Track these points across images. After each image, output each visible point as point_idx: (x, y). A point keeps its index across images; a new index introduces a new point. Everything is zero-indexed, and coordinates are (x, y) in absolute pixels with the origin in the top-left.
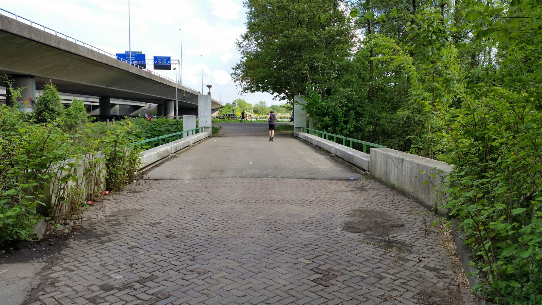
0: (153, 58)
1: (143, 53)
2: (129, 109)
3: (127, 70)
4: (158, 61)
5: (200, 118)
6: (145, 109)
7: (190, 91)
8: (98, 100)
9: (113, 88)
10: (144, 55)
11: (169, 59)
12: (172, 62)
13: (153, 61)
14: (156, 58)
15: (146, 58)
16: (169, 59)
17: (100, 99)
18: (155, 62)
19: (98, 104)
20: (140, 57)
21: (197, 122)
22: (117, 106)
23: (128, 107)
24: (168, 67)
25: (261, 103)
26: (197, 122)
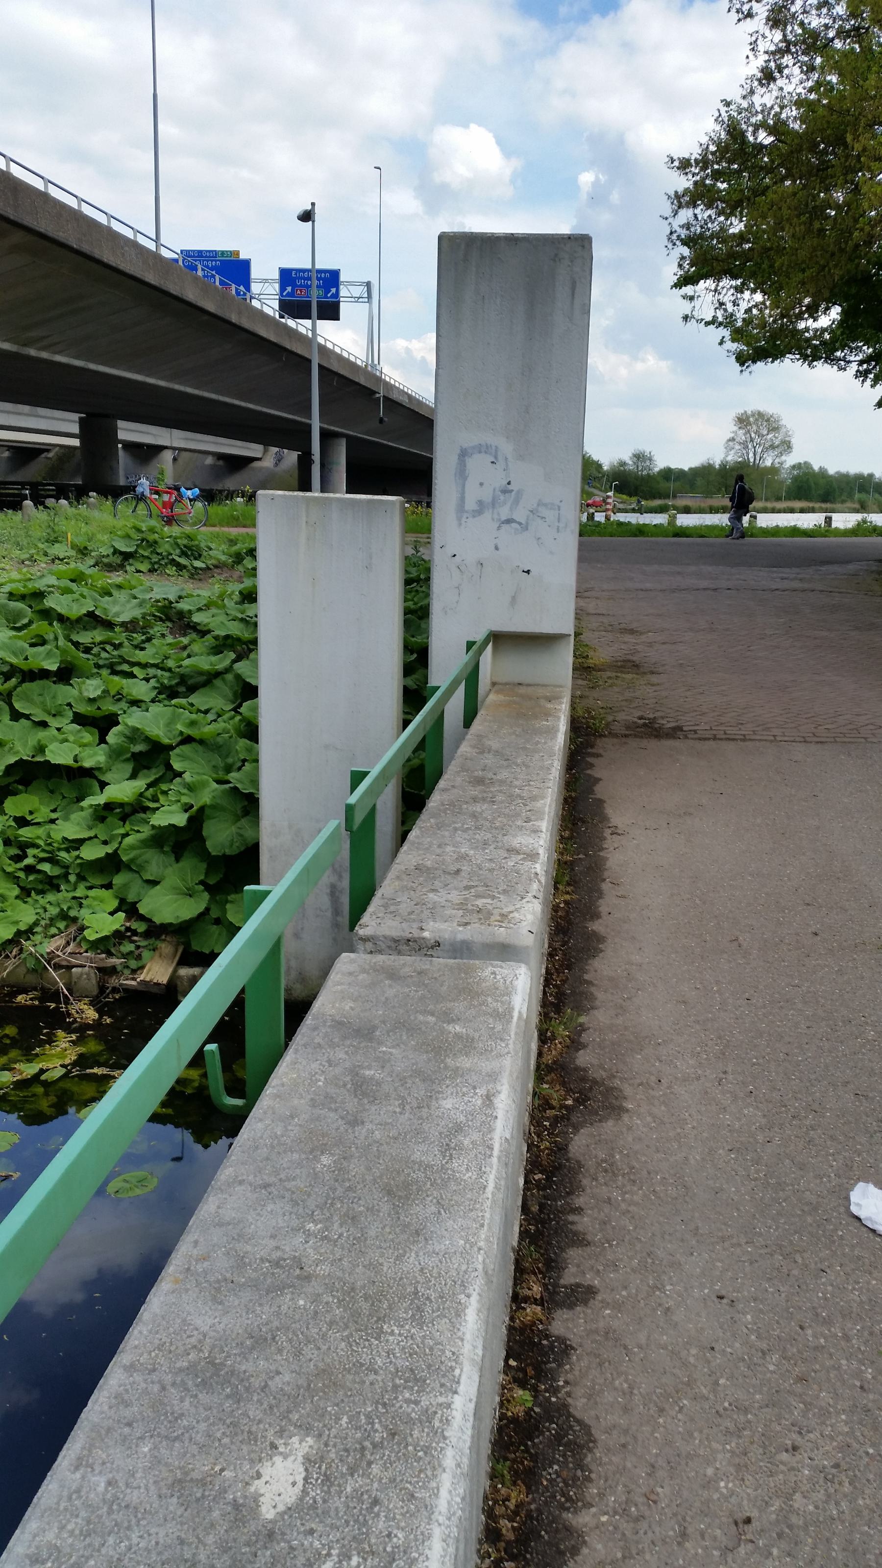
0: (276, 276)
1: (243, 256)
2: (212, 467)
3: (86, 248)
4: (294, 286)
5: (458, 535)
6: (261, 468)
7: (405, 401)
8: (75, 429)
9: (58, 358)
10: (245, 265)
11: (331, 279)
12: (343, 292)
13: (277, 286)
14: (287, 276)
15: (254, 273)
16: (331, 279)
17: (82, 422)
18: (282, 289)
19: (76, 442)
20: (236, 269)
21: (417, 582)
22: (168, 456)
23: (209, 460)
24: (330, 311)
25: (639, 457)
26: (417, 582)
